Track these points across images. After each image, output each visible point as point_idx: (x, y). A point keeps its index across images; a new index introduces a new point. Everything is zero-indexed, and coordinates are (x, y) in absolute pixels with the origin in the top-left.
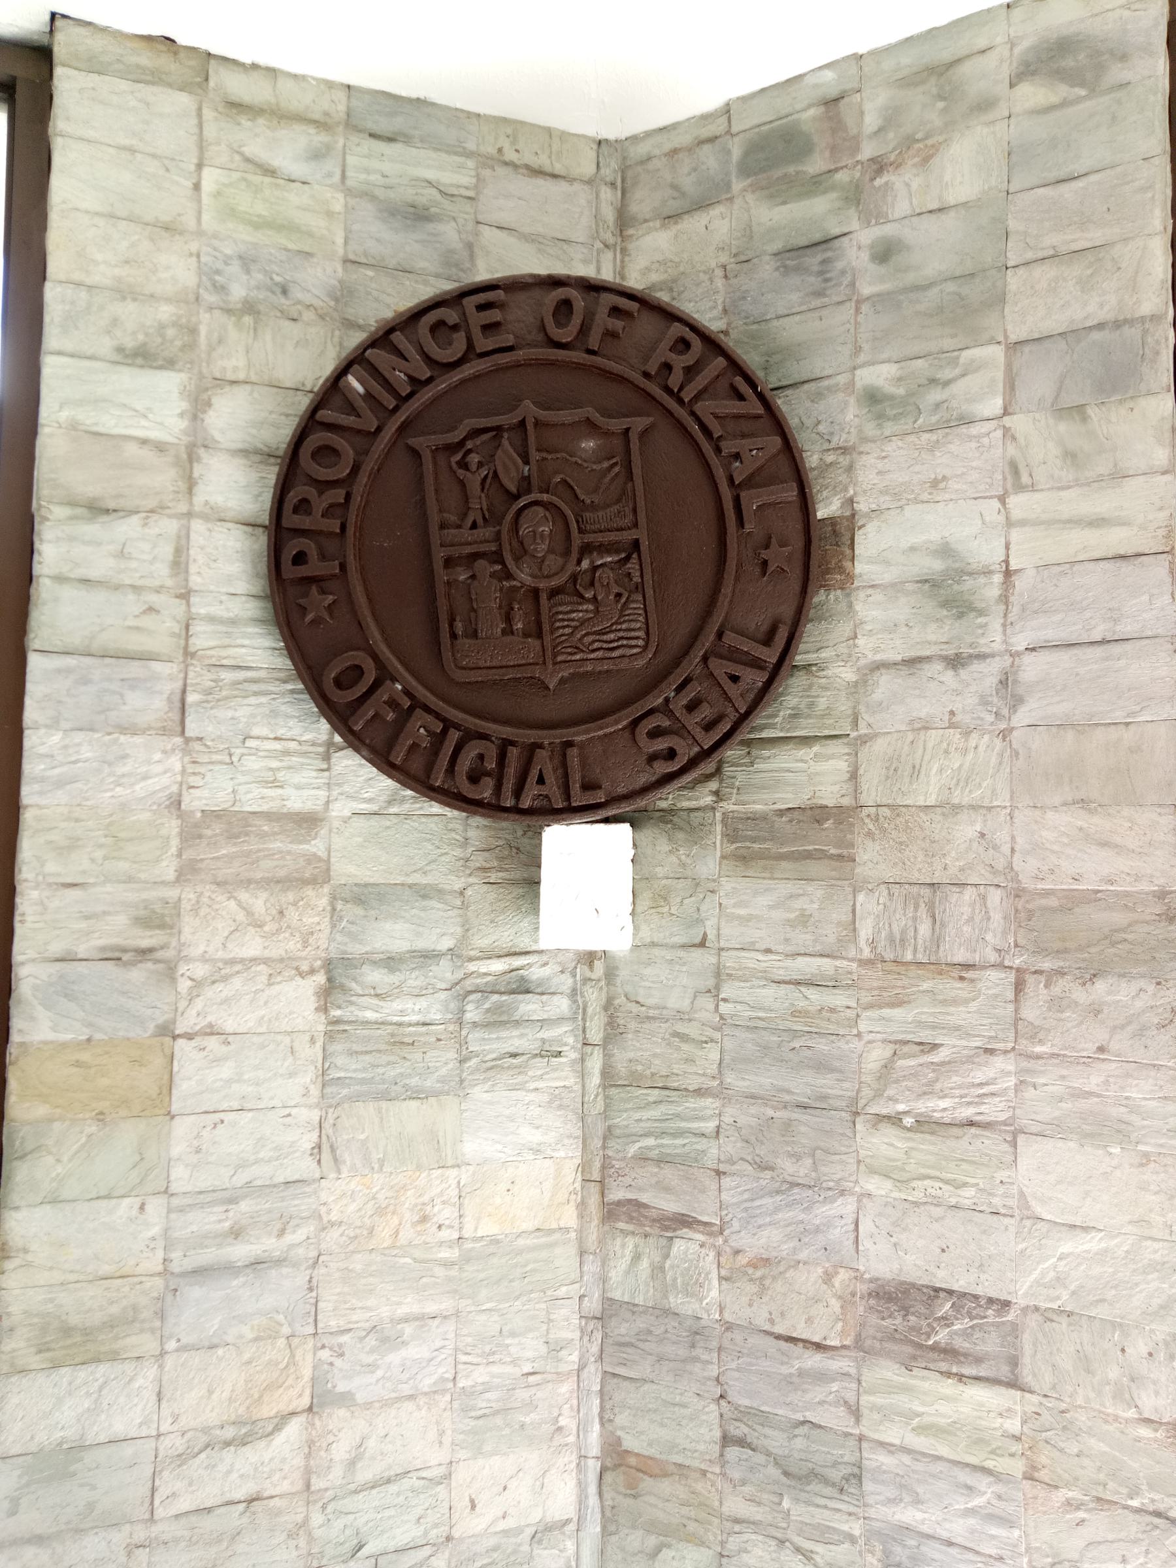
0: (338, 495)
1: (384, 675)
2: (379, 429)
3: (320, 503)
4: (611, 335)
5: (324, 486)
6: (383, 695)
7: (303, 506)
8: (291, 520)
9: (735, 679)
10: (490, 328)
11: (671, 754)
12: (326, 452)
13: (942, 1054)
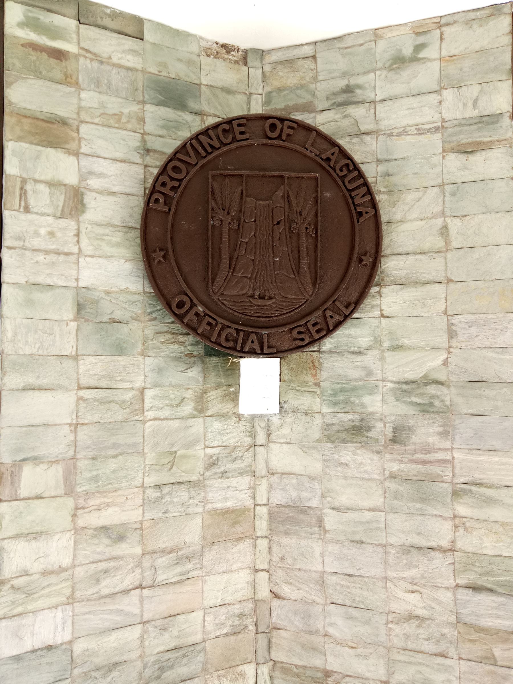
0: (176, 184)
1: (193, 305)
2: (196, 165)
3: (171, 184)
4: (289, 135)
5: (172, 179)
6: (193, 311)
7: (164, 184)
8: (158, 188)
9: (331, 317)
10: (242, 133)
11: (302, 340)
12: (175, 169)
13: (130, 395)
